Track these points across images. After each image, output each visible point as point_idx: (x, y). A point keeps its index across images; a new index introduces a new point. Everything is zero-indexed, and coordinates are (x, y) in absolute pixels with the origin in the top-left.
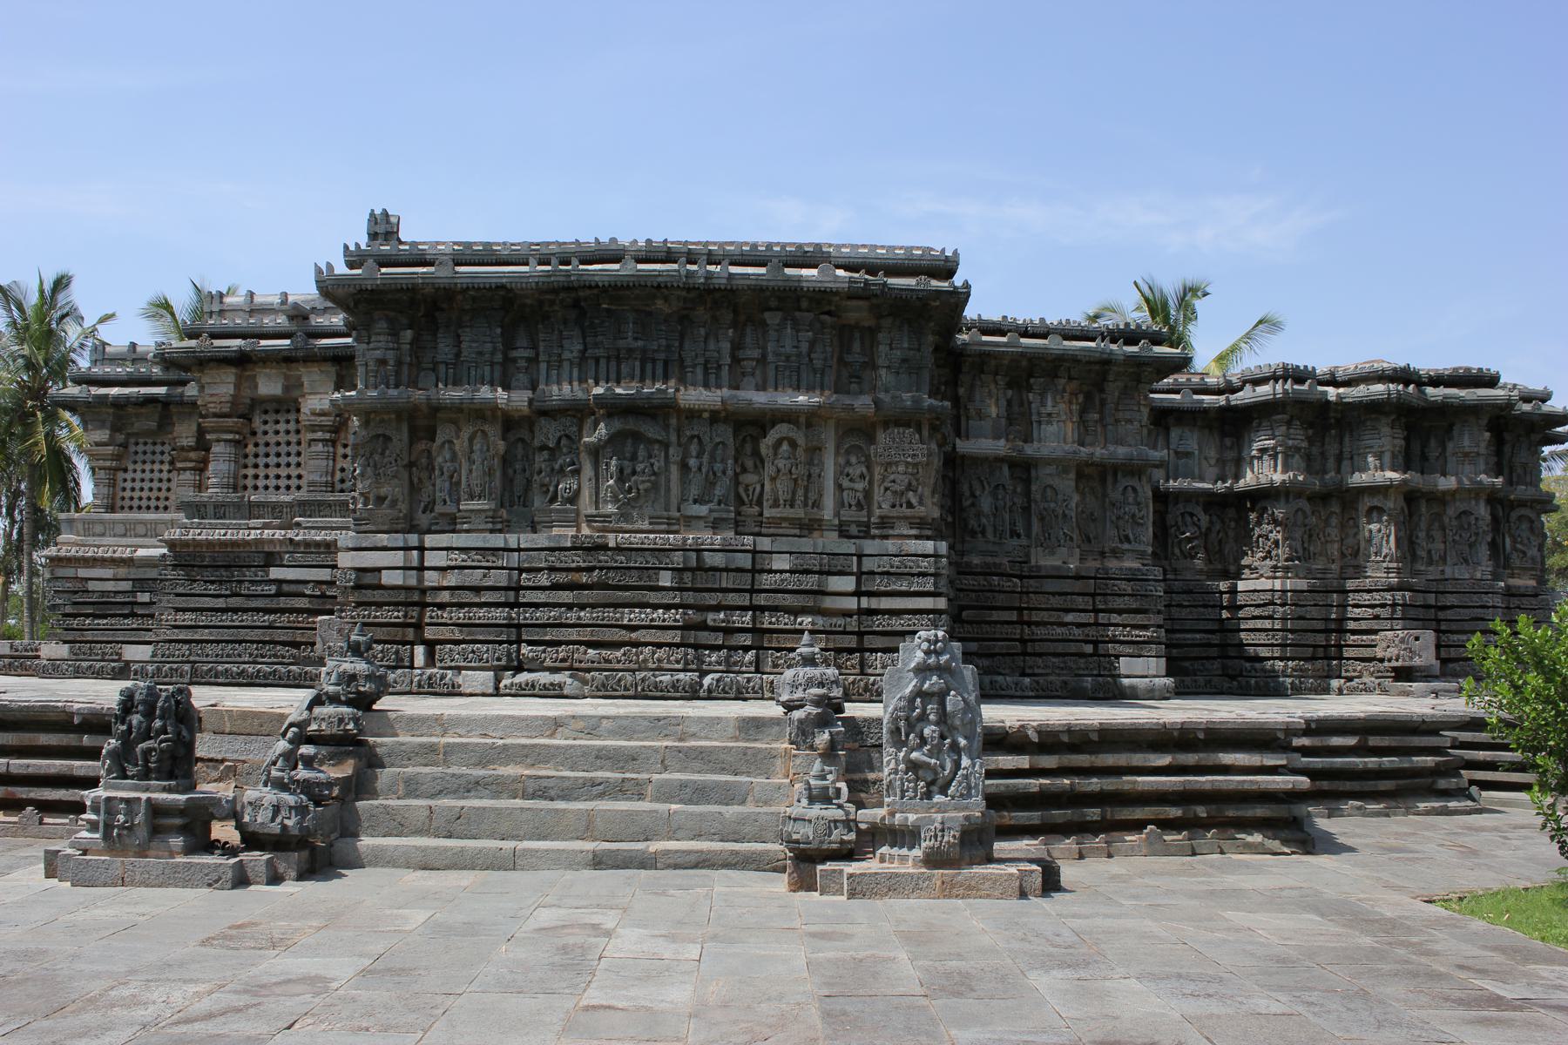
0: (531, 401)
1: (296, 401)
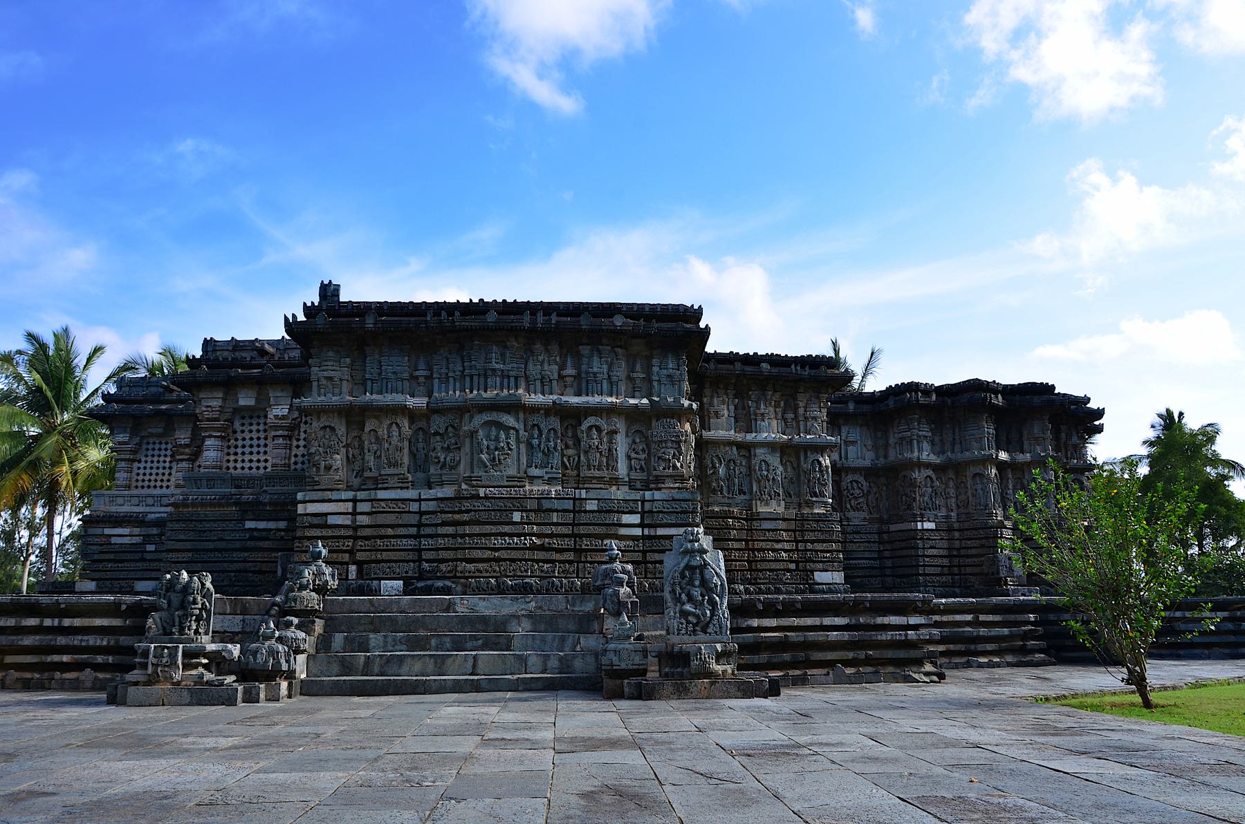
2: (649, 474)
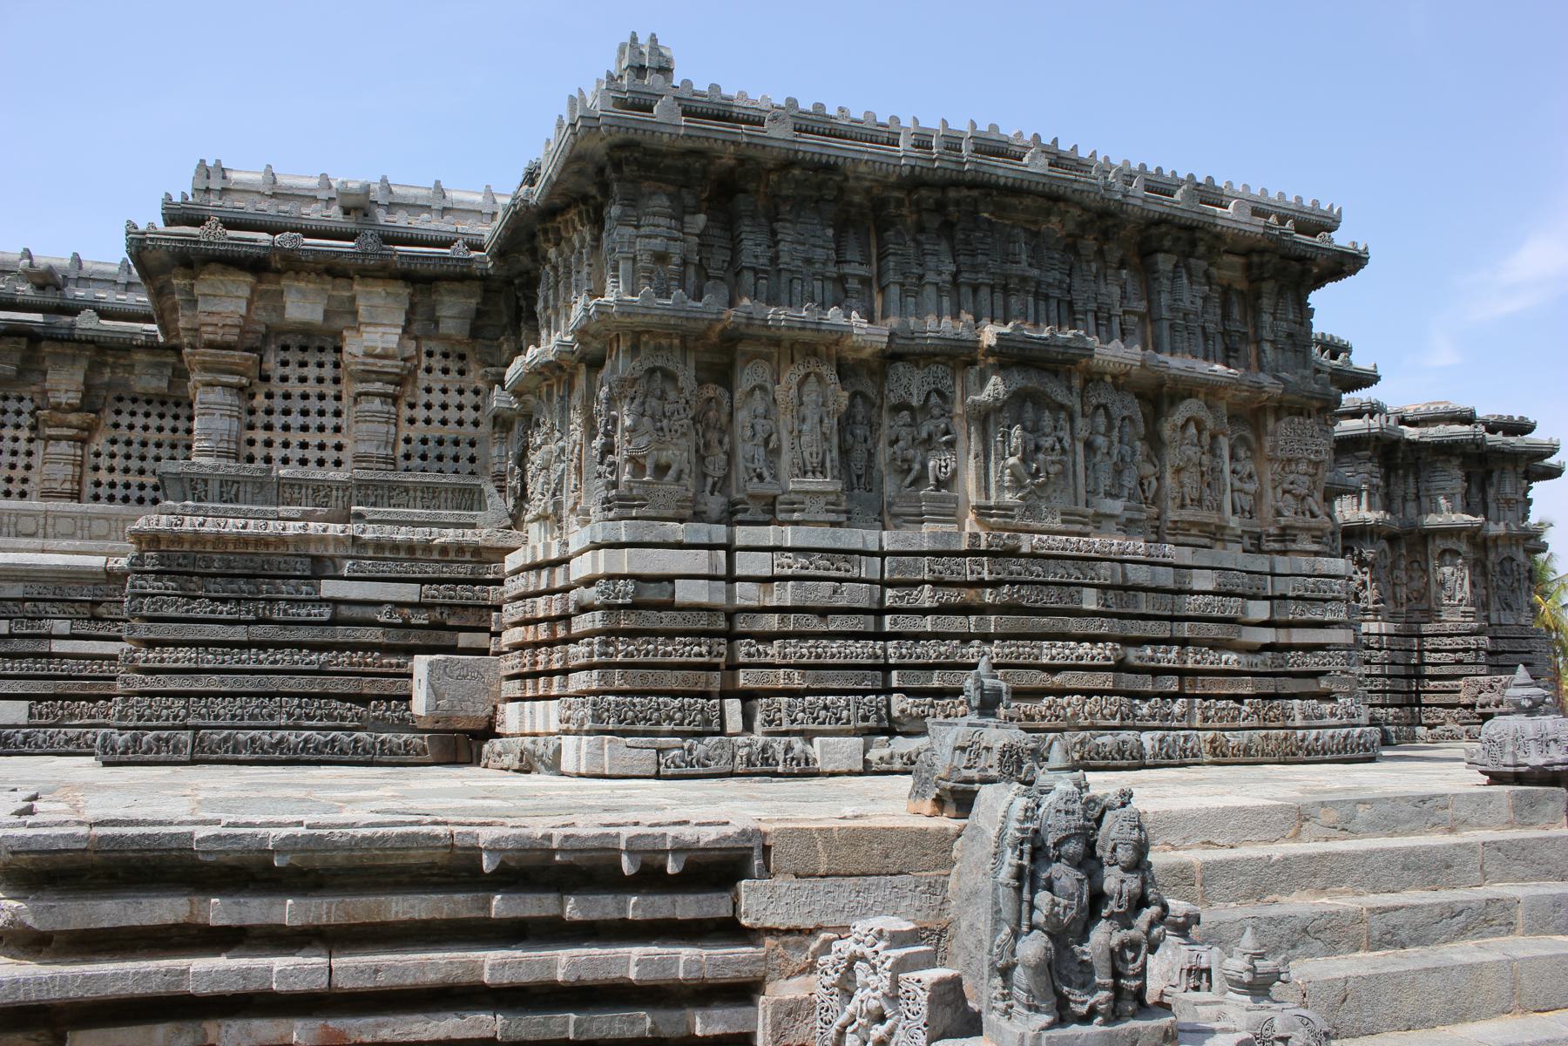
1: (338, 335)
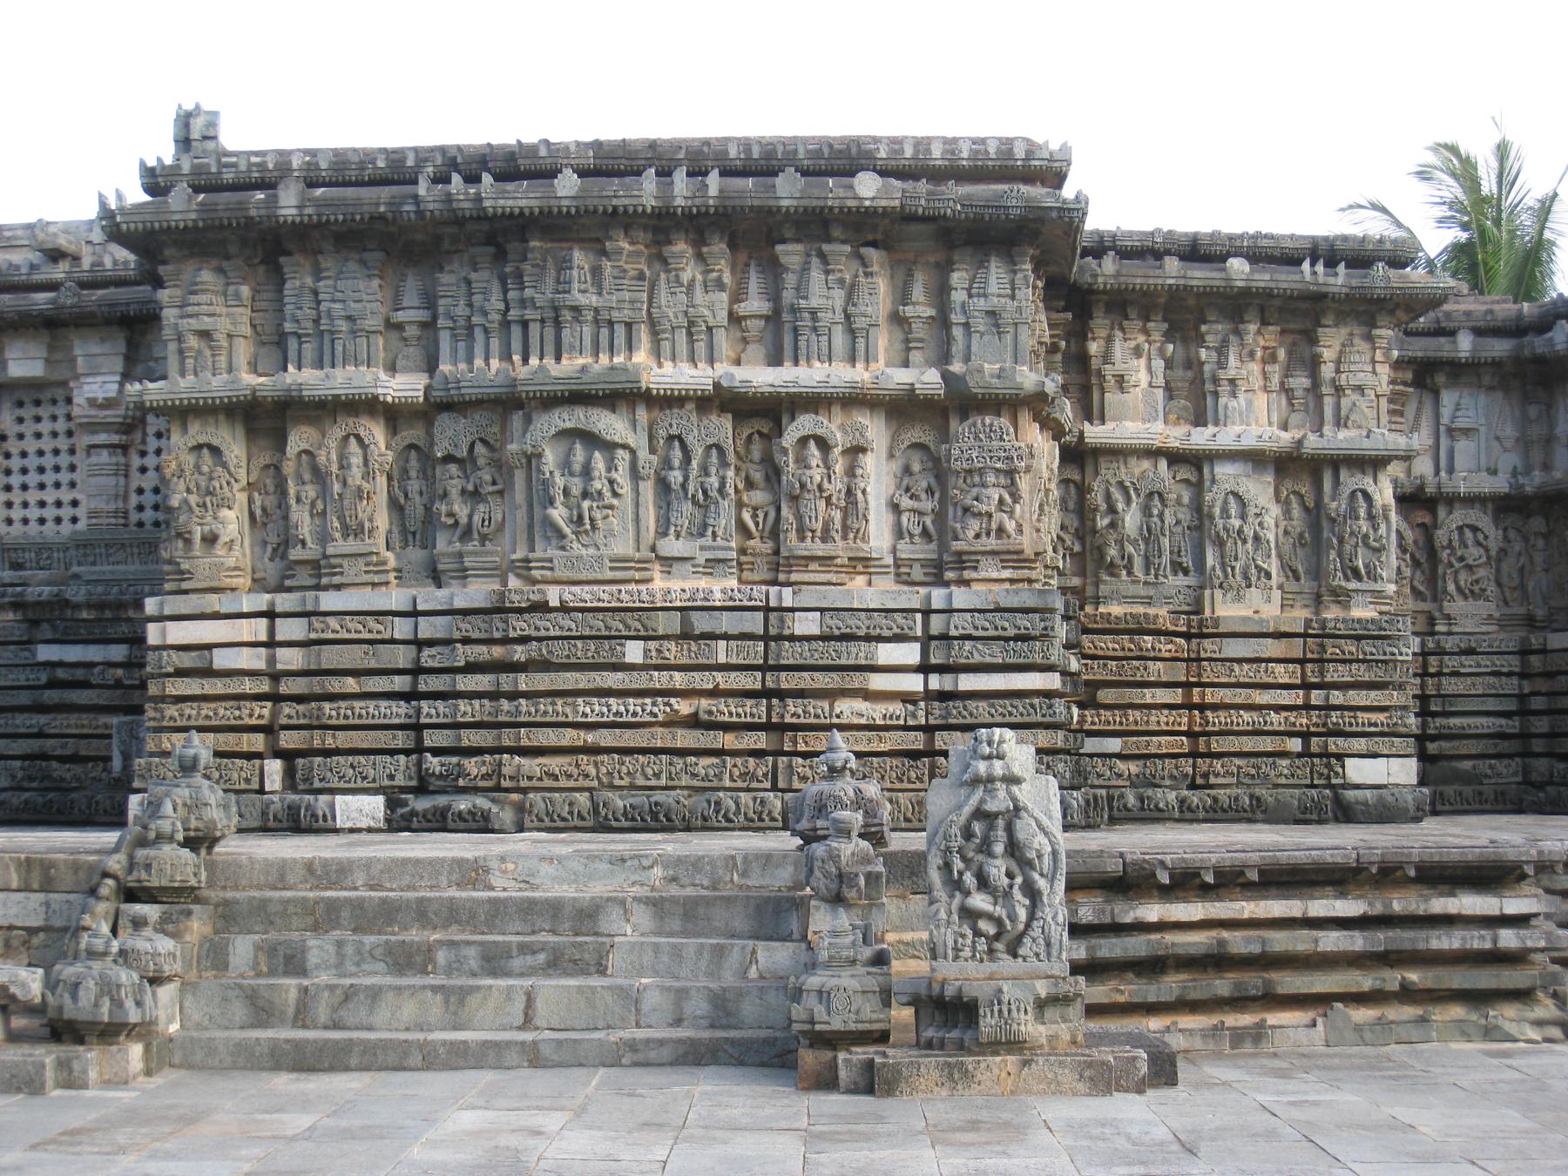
0: (428, 389)
2: (943, 547)
